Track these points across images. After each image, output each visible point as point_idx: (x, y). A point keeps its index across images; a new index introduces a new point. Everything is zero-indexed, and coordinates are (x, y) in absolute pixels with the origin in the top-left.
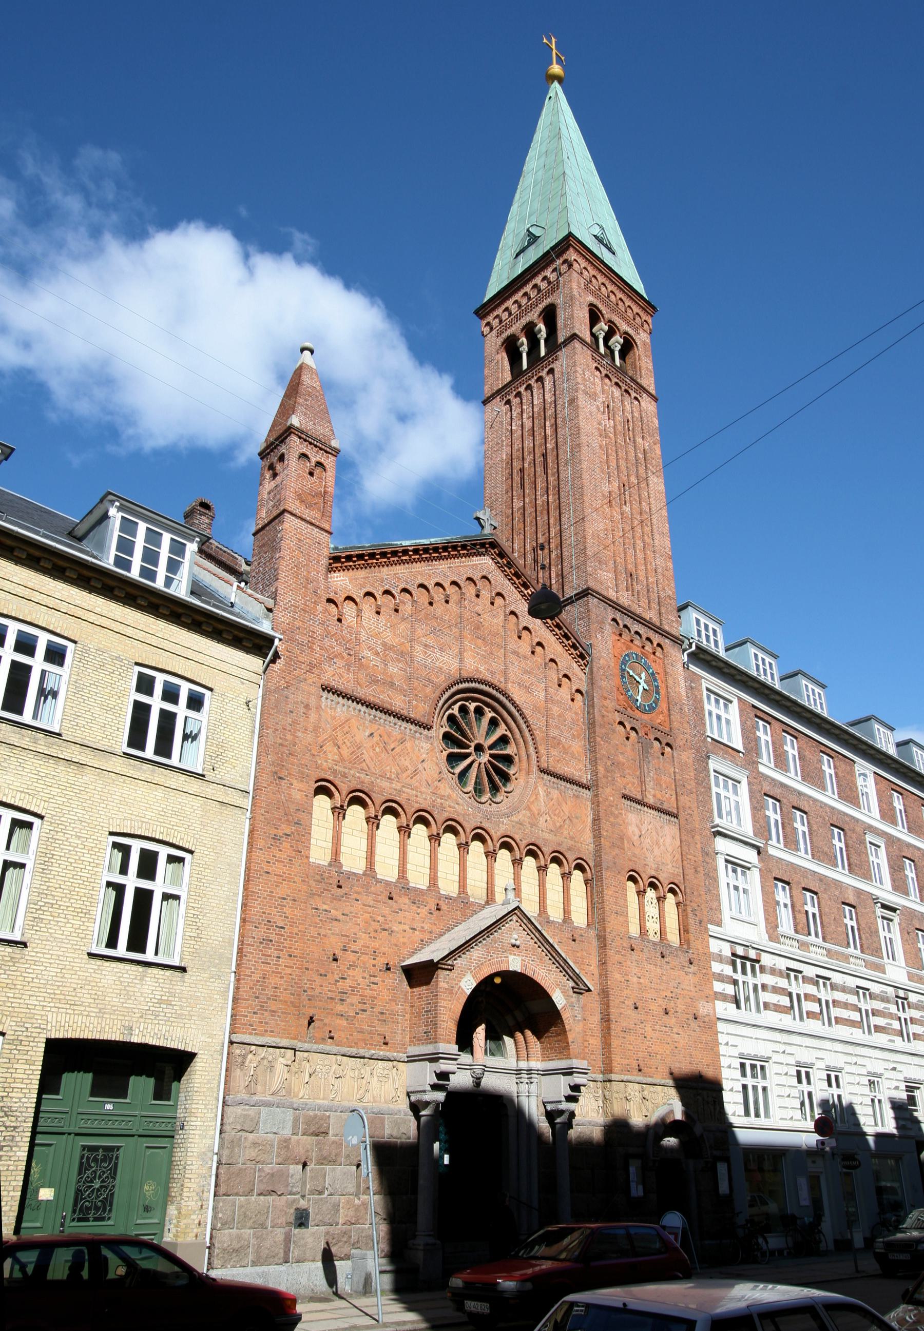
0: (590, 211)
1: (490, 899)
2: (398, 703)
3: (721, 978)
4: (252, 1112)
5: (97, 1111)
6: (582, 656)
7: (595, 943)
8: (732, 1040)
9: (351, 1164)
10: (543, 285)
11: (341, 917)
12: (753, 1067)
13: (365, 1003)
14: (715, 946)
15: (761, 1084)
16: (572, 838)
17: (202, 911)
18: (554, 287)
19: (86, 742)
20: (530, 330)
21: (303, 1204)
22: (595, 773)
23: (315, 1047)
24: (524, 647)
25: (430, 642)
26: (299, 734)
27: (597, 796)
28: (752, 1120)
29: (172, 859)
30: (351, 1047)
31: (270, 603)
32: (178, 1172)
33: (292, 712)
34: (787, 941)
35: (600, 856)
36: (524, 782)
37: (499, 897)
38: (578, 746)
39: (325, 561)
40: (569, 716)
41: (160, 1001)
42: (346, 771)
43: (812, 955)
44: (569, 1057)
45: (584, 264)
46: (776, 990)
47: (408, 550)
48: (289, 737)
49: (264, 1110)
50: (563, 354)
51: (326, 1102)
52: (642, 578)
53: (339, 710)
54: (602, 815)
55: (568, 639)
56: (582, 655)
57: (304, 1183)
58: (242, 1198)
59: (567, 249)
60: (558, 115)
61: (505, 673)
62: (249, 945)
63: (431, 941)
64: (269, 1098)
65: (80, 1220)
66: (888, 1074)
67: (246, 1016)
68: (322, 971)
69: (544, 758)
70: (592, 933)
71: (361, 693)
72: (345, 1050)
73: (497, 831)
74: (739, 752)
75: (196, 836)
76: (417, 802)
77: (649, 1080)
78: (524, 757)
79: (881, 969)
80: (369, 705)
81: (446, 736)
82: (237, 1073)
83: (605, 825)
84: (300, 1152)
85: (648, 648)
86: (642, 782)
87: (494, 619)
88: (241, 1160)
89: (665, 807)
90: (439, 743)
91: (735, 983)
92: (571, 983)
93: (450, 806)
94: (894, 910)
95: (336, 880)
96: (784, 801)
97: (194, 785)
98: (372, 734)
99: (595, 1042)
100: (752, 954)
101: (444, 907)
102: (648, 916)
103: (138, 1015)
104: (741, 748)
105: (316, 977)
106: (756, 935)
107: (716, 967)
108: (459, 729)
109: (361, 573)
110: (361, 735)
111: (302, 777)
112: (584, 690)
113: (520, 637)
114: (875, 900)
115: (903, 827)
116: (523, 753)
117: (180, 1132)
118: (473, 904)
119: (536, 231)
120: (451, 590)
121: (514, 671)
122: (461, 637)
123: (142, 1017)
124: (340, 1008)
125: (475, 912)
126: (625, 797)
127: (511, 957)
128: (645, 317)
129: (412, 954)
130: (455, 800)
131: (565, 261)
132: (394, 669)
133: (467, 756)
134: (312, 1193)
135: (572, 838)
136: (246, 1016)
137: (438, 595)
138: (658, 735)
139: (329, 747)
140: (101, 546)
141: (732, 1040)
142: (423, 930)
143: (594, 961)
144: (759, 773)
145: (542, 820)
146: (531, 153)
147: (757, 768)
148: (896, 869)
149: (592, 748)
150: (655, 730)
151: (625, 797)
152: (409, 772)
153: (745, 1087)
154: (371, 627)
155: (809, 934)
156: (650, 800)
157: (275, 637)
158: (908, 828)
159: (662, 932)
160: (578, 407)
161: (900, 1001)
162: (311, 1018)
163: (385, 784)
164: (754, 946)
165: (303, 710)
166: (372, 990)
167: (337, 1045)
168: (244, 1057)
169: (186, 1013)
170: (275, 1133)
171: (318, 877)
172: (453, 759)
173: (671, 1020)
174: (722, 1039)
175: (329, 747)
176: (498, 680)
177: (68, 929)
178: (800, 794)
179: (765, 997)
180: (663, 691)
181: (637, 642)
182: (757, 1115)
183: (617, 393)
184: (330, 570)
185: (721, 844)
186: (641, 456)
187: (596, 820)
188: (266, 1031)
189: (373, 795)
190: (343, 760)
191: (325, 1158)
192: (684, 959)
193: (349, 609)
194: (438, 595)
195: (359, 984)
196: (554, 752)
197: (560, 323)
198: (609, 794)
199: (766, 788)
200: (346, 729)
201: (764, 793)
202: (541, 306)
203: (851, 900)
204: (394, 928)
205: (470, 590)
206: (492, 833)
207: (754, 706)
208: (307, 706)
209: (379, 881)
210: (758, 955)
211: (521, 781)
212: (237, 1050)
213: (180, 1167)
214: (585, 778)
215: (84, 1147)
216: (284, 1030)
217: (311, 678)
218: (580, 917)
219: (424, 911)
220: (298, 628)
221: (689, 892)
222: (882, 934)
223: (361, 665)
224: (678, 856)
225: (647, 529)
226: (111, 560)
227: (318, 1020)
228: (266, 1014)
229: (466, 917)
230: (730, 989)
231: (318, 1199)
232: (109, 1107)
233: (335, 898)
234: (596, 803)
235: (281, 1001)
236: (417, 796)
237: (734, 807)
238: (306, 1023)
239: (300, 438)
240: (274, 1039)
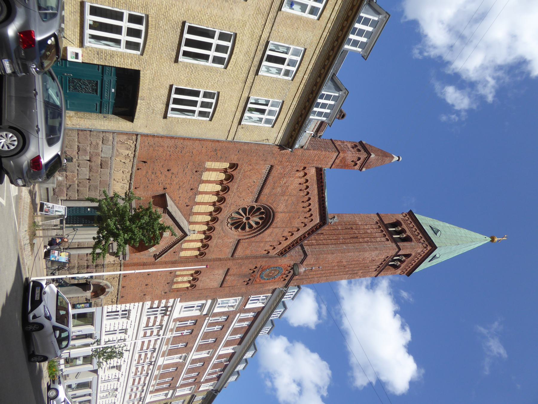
0: (443, 254)
1: (190, 223)
2: (266, 191)
3: (160, 303)
4: (110, 143)
5: (112, 85)
6: (282, 253)
7: (174, 259)
8: (136, 307)
10: (419, 237)
11: (185, 172)
12: (126, 314)
14: (171, 301)
16: (213, 251)
17: (189, 125)
18: (418, 241)
19: (254, 84)
20: (403, 231)
21: (74, 160)
22: (238, 259)
23: (135, 163)
24: (286, 234)
25: (289, 202)
27: (229, 260)
28: (105, 314)
31: (305, 147)
35: (206, 261)
36: (235, 234)
37: (191, 227)
38: (248, 252)
39: (320, 166)
40: (260, 249)
44: (130, 253)
45: (426, 252)
46: (155, 322)
49: (111, 147)
50: (394, 245)
52: (310, 273)
54: (222, 262)
55: (288, 249)
56: (282, 253)
57: (82, 160)
59: (431, 246)
60: (480, 240)
61: (276, 227)
63: (175, 204)
64: (115, 149)
65: (69, 80)
66: (121, 373)
68: (164, 166)
69: (244, 241)
70: (177, 258)
71: (270, 178)
72: (134, 174)
73: (217, 225)
77: (121, 280)
78: (244, 234)
79: (163, 356)
81: (253, 207)
82: (125, 137)
83: (218, 263)
84: (93, 159)
85: (285, 276)
86: (234, 275)
87: (297, 223)
88: (91, 139)
89: (225, 283)
90: (251, 204)
91: (158, 307)
92: (158, 253)
94: (184, 360)
95: (199, 170)
96: (226, 322)
97: (236, 121)
99: (136, 261)
100: (168, 313)
101: (188, 208)
102: (183, 274)
105: (162, 164)
106: (176, 315)
107: (164, 301)
108: (255, 212)
109: (315, 178)
110: (254, 178)
111: (239, 159)
112: (270, 254)
113: (290, 232)
114: (188, 354)
116: (246, 234)
118: (189, 218)
119: (439, 234)
120: (308, 209)
121: (277, 230)
122: (290, 212)
125: (186, 218)
126: (228, 269)
127: (168, 233)
128: (406, 272)
129: (170, 197)
130: (228, 211)
131: (427, 246)
132: (279, 189)
133: (246, 214)
134: (78, 163)
135: (213, 251)
137: (306, 204)
138: (252, 280)
140: (329, 89)
141: (136, 307)
142: (179, 200)
143: (167, 260)
145: (221, 241)
146: (467, 231)
148: (200, 360)
149: (247, 258)
150: (251, 281)
151: (228, 269)
153: (118, 311)
154: (295, 182)
156: (227, 278)
159: (178, 283)
160: (374, 251)
163: (236, 187)
168: (132, 140)
171: (200, 164)
172: (244, 210)
173: (144, 286)
174: (136, 304)
175: (250, 167)
176: (274, 224)
177: (182, 77)
178: (229, 327)
179: (152, 318)
180: (268, 281)
181: (287, 272)
182: (107, 316)
183: (378, 264)
184: (317, 168)
185: (210, 301)
186: (355, 272)
187: (220, 260)
189: (231, 183)
190: (245, 172)
192: (167, 290)
193: (302, 174)
194: (306, 204)
196: (246, 244)
197: (406, 244)
198: (230, 264)
199: (231, 316)
201: (229, 316)
202: (411, 236)
203: (189, 346)
205: (308, 215)
206: (216, 224)
208: (265, 160)
209: (198, 186)
211: (236, 233)
212: (134, 137)
214: (236, 255)
215: (97, 82)
217: (276, 162)
218: (183, 254)
219: (187, 201)
221: (193, 290)
222: (176, 356)
223: (281, 178)
224: (206, 288)
225: (329, 275)
226: (323, 92)
229: (184, 215)
230: (155, 306)
232: (113, 90)
233: (192, 170)
234: (226, 260)
237: (226, 304)
238: (144, 160)
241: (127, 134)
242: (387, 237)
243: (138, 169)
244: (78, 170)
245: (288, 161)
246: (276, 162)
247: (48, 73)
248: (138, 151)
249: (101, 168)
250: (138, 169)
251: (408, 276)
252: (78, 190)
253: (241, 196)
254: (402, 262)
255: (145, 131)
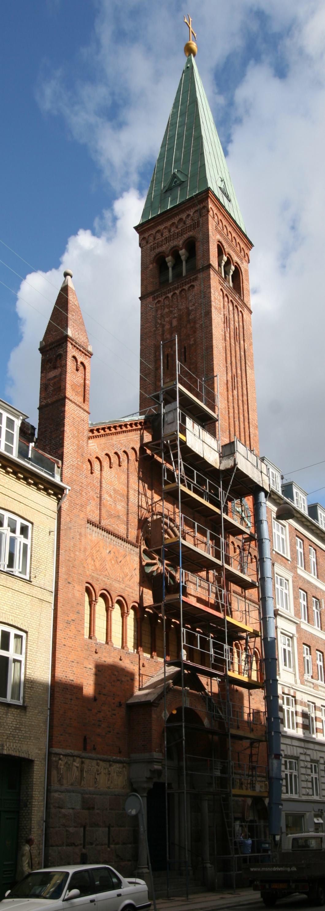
13: (110, 727)
15: (295, 773)
26: (77, 553)
29: (17, 636)
32: (24, 833)
33: (73, 538)
34: (308, 684)
41: (16, 728)
42: (98, 576)
43: (320, 692)
47: (127, 424)
48: (72, 555)
53: (94, 535)
74: (288, 560)
75: (29, 622)
76: (132, 597)
80: (109, 532)
93: (148, 599)
96: (309, 592)
98: (110, 552)
103: (6, 737)
104: (289, 558)
109: (103, 440)
115: (314, 575)
117: (24, 809)
123: (7, 738)
139: (89, 560)
144: (297, 574)
147: (296, 571)
152: (128, 577)
155: (318, 679)
157: (66, 489)
158: (317, 576)
161: (285, 696)
162: (85, 737)
164: (294, 687)
165: (78, 537)
169: (28, 735)
170: (73, 809)
171: (86, 647)
178: (317, 587)
182: (292, 793)
190: (96, 569)
199: (301, 585)
200: (98, 549)
201: (302, 587)
202: (185, 236)
204: (123, 679)
207: (296, 529)
208: (80, 534)
210: (295, 693)
213: (27, 830)
217: (82, 515)
220: (75, 481)
236: (132, 593)
239: (72, 344)
240: (71, 751)
241: (51, 766)
242: (186, 287)
243: (95, 749)
244: (97, 845)
245: (81, 494)
246: (82, 515)
247: (298, 702)
248: (73, 751)
249: (93, 808)
250: (95, 749)
251: (252, 245)
252: (124, 844)
253: (130, 574)
254: (228, 263)
255: (45, 740)
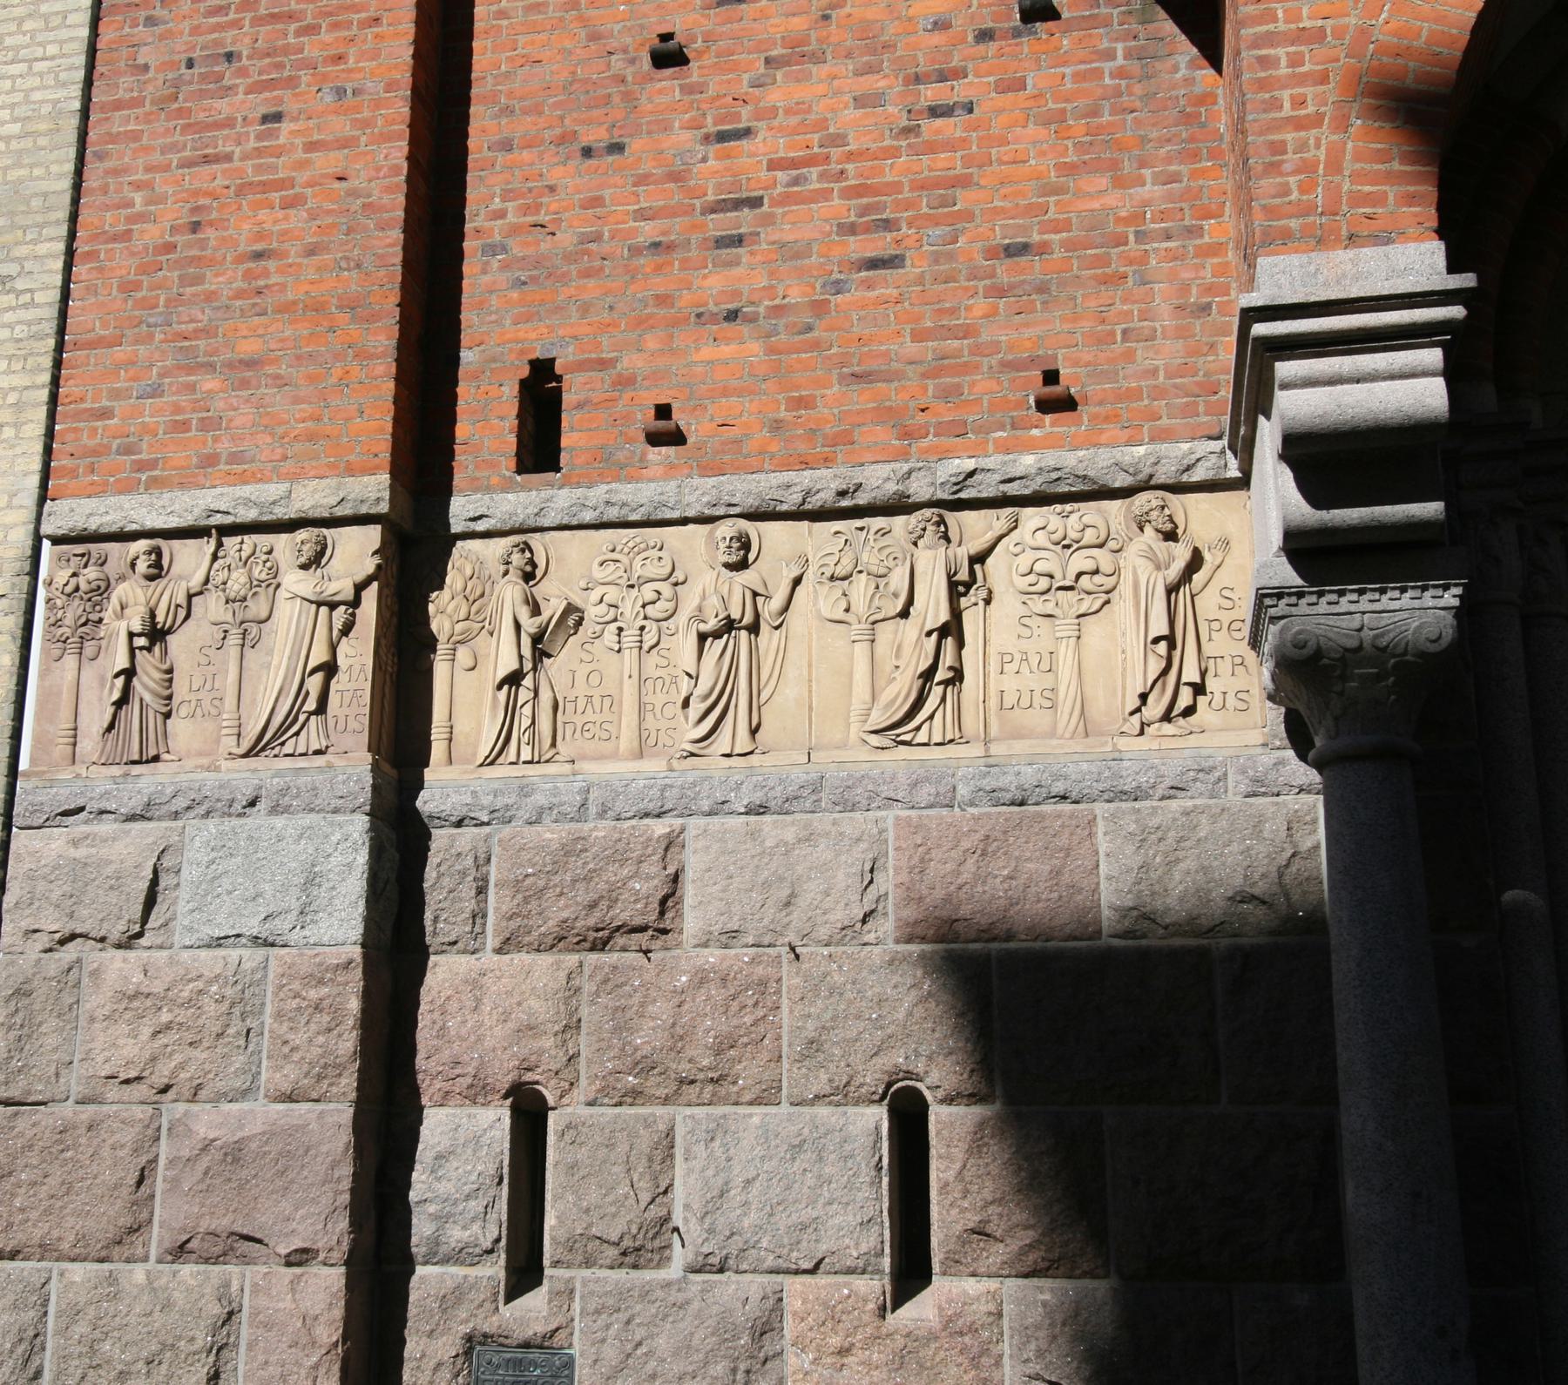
9: (842, 1094)
13: (888, 225)
30: (806, 465)
51: (653, 766)
58: (78, 1272)
62: (118, 105)
67: (105, 414)
88: (74, 1083)
124: (713, 285)
136: (105, 414)
166: (931, 148)
167: (709, 470)
188: (211, 460)
191: (644, 1067)
195: (838, 140)
216: (311, 437)
227: (581, 366)
228: (209, 383)
231: (623, 1294)
235: (286, 308)
240: (247, 491)
